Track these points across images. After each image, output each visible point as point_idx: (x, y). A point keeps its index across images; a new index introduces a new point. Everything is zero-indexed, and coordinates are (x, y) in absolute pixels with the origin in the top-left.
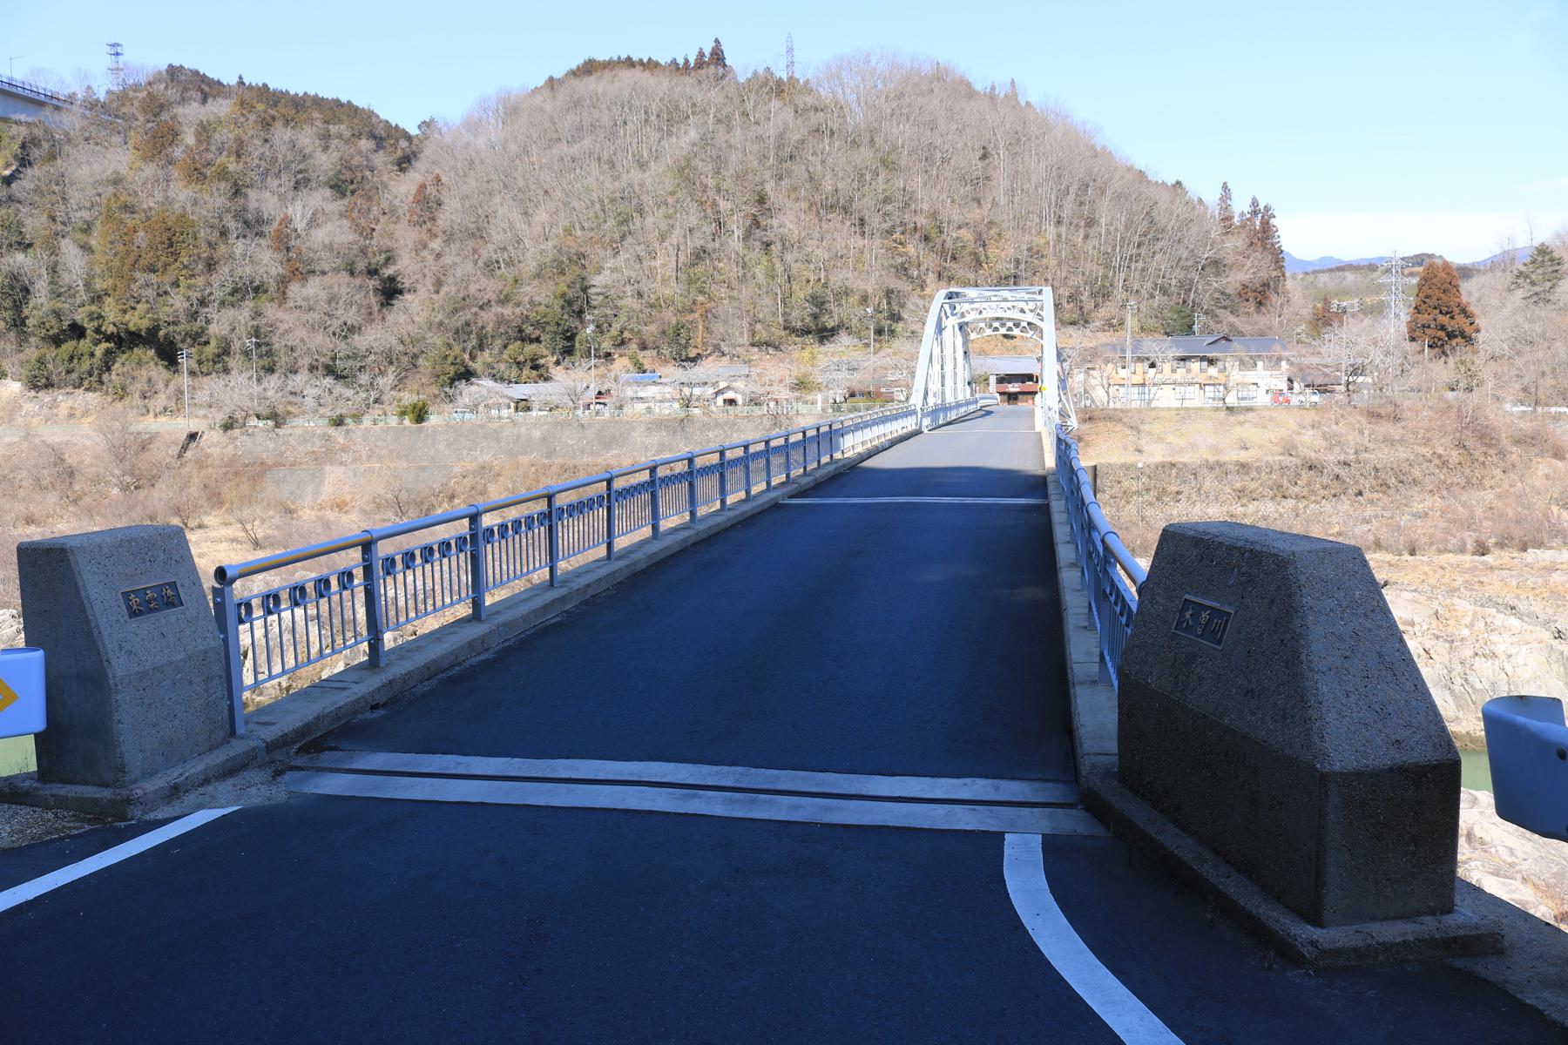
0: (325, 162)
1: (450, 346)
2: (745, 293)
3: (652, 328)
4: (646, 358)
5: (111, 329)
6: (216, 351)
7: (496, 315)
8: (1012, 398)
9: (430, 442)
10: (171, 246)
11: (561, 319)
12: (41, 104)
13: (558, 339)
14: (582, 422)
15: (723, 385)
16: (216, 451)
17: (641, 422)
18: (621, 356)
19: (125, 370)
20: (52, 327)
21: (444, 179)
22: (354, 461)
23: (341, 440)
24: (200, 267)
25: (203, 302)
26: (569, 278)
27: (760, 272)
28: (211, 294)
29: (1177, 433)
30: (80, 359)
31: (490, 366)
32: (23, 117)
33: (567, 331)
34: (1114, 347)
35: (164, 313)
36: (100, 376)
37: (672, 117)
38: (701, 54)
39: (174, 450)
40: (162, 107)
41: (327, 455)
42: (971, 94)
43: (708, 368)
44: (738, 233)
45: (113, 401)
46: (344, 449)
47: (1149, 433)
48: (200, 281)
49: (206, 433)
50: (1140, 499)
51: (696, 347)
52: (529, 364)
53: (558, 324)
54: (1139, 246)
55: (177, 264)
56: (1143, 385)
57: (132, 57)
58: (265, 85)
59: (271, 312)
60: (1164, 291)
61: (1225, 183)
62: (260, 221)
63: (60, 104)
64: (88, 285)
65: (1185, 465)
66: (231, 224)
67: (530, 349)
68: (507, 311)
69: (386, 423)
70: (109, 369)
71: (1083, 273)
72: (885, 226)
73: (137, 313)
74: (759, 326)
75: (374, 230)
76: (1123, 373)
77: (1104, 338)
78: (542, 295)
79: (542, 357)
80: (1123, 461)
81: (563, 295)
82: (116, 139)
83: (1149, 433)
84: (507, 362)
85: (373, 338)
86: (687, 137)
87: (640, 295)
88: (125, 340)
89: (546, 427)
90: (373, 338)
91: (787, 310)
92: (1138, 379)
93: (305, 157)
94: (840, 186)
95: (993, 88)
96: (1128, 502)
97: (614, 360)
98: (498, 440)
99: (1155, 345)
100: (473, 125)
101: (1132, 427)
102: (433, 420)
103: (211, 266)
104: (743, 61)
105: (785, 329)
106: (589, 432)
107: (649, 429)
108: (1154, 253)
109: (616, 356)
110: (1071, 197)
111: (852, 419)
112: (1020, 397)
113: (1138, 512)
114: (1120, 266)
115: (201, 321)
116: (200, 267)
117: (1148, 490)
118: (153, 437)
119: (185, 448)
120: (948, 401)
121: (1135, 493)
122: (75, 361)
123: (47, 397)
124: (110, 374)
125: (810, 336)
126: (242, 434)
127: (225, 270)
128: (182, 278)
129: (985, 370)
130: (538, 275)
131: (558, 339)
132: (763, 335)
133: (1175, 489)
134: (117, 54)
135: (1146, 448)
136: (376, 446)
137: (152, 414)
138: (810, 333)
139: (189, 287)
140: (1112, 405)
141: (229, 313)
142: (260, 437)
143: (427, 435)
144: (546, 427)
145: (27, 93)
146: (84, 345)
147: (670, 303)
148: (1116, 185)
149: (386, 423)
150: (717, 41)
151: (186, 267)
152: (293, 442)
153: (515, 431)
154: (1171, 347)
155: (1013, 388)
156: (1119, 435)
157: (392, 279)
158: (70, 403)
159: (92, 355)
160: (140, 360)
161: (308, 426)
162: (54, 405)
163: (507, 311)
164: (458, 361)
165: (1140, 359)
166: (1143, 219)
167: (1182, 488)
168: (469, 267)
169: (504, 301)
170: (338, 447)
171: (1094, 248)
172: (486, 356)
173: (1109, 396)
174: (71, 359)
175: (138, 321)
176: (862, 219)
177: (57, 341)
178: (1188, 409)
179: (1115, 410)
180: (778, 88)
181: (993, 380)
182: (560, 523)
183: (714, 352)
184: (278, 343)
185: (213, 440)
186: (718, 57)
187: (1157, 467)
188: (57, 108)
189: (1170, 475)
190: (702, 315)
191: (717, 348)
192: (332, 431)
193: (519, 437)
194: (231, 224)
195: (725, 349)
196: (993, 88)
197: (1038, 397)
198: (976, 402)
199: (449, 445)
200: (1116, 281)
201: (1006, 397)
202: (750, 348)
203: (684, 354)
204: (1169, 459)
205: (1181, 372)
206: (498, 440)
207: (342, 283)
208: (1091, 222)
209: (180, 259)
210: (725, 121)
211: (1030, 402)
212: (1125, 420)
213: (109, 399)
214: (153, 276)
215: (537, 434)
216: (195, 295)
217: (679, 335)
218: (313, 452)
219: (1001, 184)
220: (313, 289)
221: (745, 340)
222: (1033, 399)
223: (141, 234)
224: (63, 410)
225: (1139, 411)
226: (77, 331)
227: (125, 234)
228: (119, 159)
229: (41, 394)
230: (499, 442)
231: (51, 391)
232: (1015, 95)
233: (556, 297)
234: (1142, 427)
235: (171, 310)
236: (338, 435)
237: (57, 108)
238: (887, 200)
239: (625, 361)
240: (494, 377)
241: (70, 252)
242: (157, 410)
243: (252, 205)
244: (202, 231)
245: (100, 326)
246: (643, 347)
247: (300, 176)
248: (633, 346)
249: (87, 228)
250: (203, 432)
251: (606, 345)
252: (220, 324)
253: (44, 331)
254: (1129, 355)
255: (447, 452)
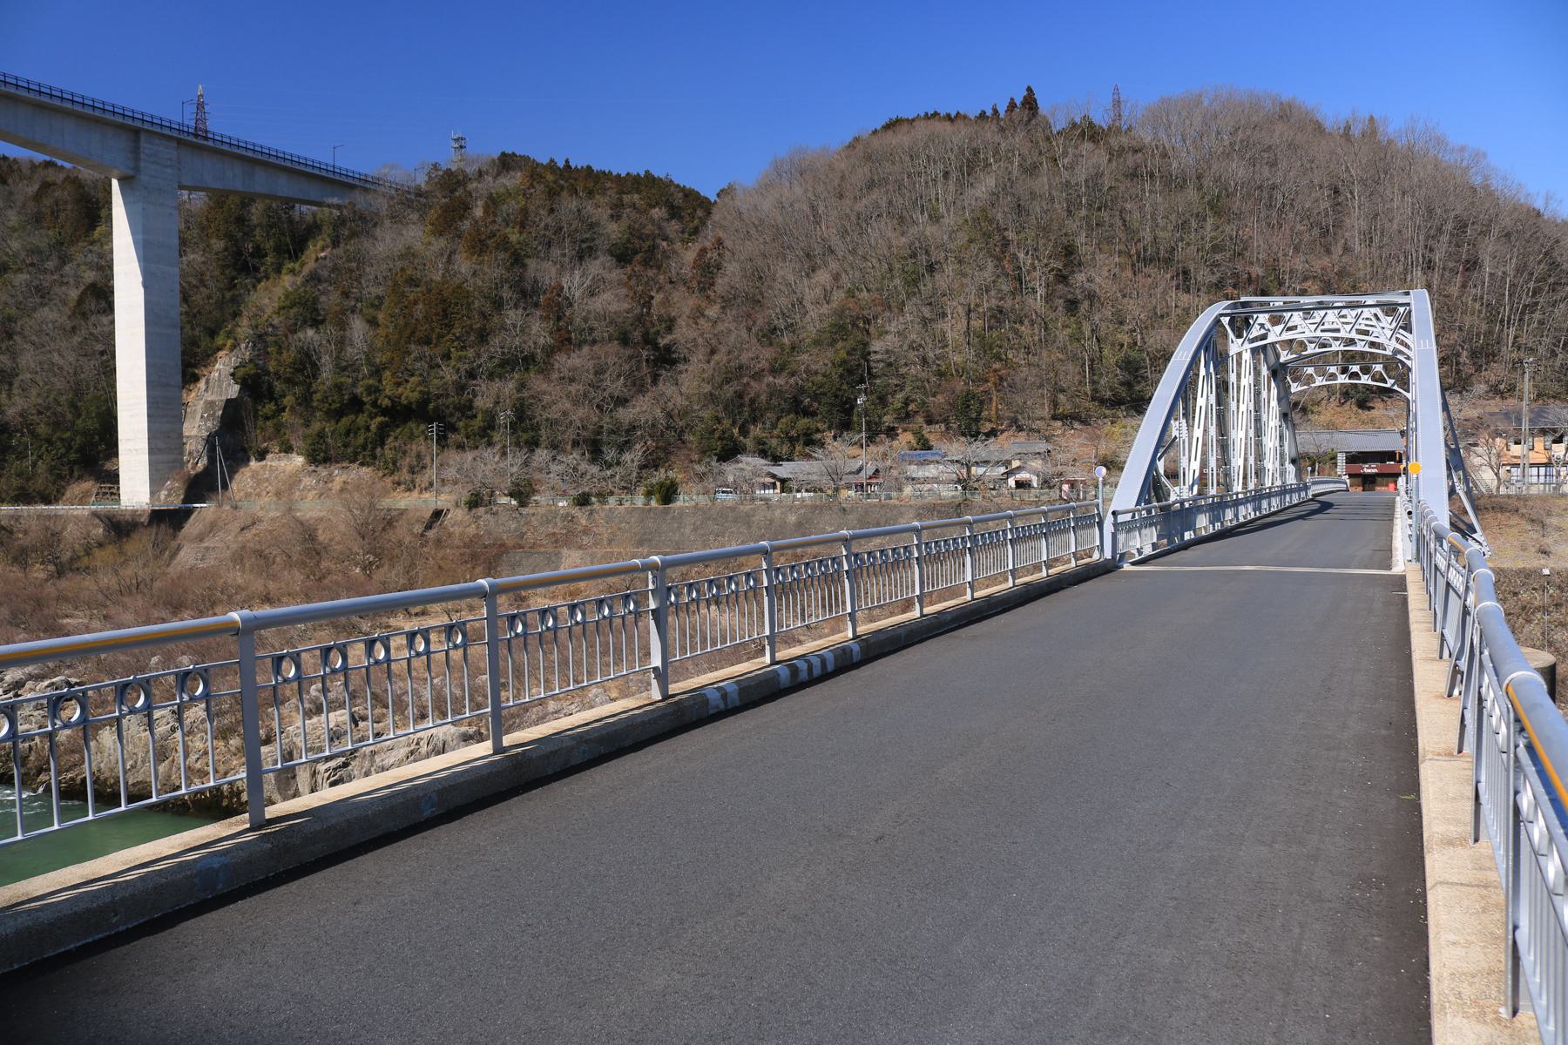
0: (614, 231)
1: (718, 420)
2: (1045, 357)
3: (940, 399)
4: (932, 433)
5: (386, 402)
6: (482, 424)
7: (768, 385)
8: (1368, 482)
9: (676, 525)
10: (445, 316)
11: (839, 389)
12: (352, 187)
14: (844, 505)
15: (1015, 464)
16: (457, 530)
17: (911, 506)
19: (397, 444)
20: (333, 401)
21: (728, 243)
22: (595, 544)
23: (584, 522)
24: (472, 338)
25: (472, 375)
26: (851, 343)
27: (1063, 336)
28: (480, 366)
30: (356, 433)
31: (760, 442)
32: (335, 201)
33: (846, 403)
34: (1507, 415)
35: (435, 385)
36: (374, 449)
37: (972, 164)
39: (418, 529)
40: (459, 183)
41: (568, 537)
42: (1319, 128)
43: (1007, 445)
44: (1041, 292)
45: (384, 475)
46: (586, 531)
47: (1559, 529)
48: (471, 353)
49: (452, 511)
50: (1546, 617)
51: (990, 421)
53: (836, 396)
54: (1534, 294)
55: (450, 336)
56: (1548, 465)
57: (473, 150)
58: (589, 168)
59: (538, 383)
62: (536, 290)
63: (368, 186)
64: (369, 362)
66: (506, 293)
67: (804, 422)
68: (780, 381)
69: (632, 503)
70: (383, 444)
71: (1460, 329)
72: (1214, 279)
73: (409, 386)
74: (1061, 397)
75: (652, 298)
76: (1516, 450)
77: (1495, 405)
78: (819, 362)
79: (818, 431)
80: (1520, 565)
81: (844, 362)
82: (415, 216)
83: (1559, 529)
84: (779, 437)
85: (642, 409)
86: (985, 185)
87: (924, 361)
88: (399, 414)
90: (642, 409)
91: (1096, 378)
93: (592, 226)
94: (1161, 234)
95: (1348, 128)
96: (1529, 621)
98: (749, 525)
101: (1533, 521)
102: (682, 502)
103: (483, 337)
104: (1057, 110)
105: (1093, 399)
107: (919, 514)
109: (900, 431)
110: (1445, 238)
111: (1045, 513)
113: (1543, 634)
114: (1509, 319)
115: (468, 393)
116: (472, 338)
117: (1557, 605)
118: (402, 512)
119: (429, 527)
120: (1268, 484)
121: (1538, 609)
122: (352, 435)
123: (323, 471)
124: (383, 448)
125: (1123, 407)
126: (486, 513)
127: (495, 341)
128: (452, 350)
130: (817, 343)
132: (1065, 406)
134: (461, 147)
136: (619, 529)
137: (418, 489)
138: (1123, 404)
139: (460, 359)
140: (1503, 490)
141: (497, 384)
142: (503, 517)
143: (673, 518)
145: (343, 179)
146: (361, 419)
147: (961, 371)
148: (1507, 222)
149: (632, 503)
150: (1029, 89)
151: (458, 338)
152: (535, 523)
153: (769, 515)
155: (1369, 469)
156: (1515, 531)
157: (668, 348)
158: (344, 477)
159: (368, 429)
160: (412, 434)
161: (553, 502)
162: (330, 479)
164: (726, 435)
165: (1544, 432)
168: (744, 333)
169: (774, 371)
170: (580, 528)
171: (1475, 300)
173: (1499, 479)
174: (348, 433)
175: (409, 393)
176: (1186, 272)
177: (338, 414)
179: (1509, 496)
180: (1090, 133)
181: (1341, 459)
184: (541, 415)
185: (457, 517)
186: (1030, 102)
188: (366, 190)
192: (576, 511)
194: (506, 293)
196: (1348, 128)
197: (1401, 481)
198: (1306, 488)
199: (695, 529)
201: (1360, 479)
202: (1052, 423)
203: (974, 428)
206: (749, 525)
207: (611, 353)
208: (1472, 265)
209: (453, 331)
210: (1031, 170)
211: (1392, 486)
213: (381, 474)
214: (426, 348)
215: (792, 518)
216: (464, 367)
218: (554, 534)
219: (1356, 222)
220: (577, 360)
221: (1046, 412)
222: (1396, 483)
223: (420, 306)
224: (337, 485)
225: (1543, 498)
226: (356, 404)
227: (406, 307)
228: (415, 234)
229: (320, 468)
230: (750, 527)
231: (328, 465)
232: (1374, 132)
234: (1548, 521)
235: (441, 383)
236: (581, 515)
237: (366, 190)
238: (1216, 249)
240: (763, 454)
241: (358, 327)
242: (423, 486)
243: (531, 273)
244: (476, 302)
245: (376, 400)
246: (930, 422)
247: (584, 246)
248: (920, 419)
249: (377, 303)
250: (448, 510)
251: (888, 420)
252: (486, 395)
253: (327, 405)
254: (1525, 426)
255: (692, 538)
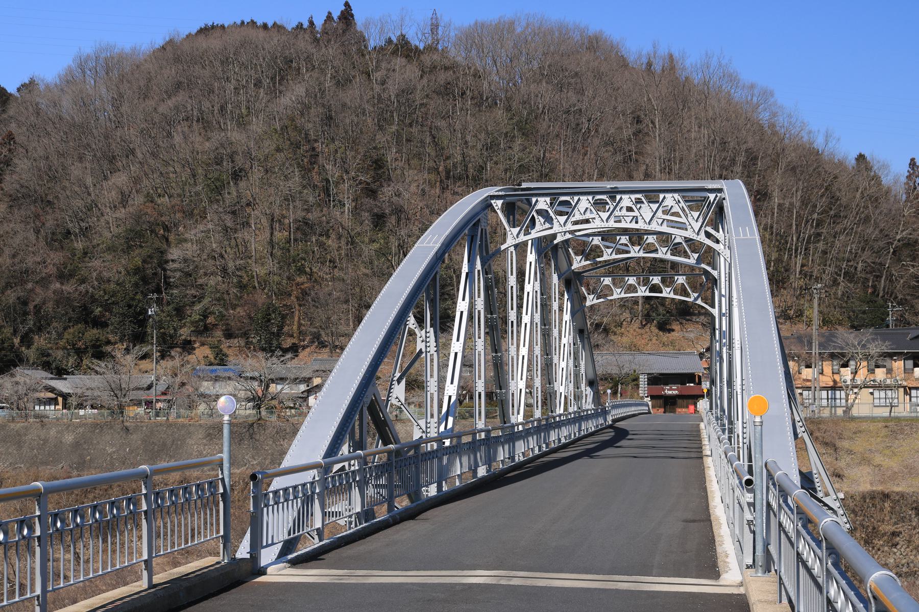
3: (240, 311)
8: (669, 403)
13: (127, 323)
17: (200, 425)
18: (203, 344)
29: (887, 452)
38: (329, 17)
51: (292, 336)
52: (91, 351)
60: (850, 276)
61: (913, 160)
65: (902, 495)
67: (93, 333)
68: (68, 288)
83: (850, 452)
84: (64, 348)
89: (81, 430)
92: (827, 380)
97: (194, 349)
98: (19, 445)
99: (846, 337)
100: (69, 81)
106: (134, 437)
107: (209, 435)
108: (836, 233)
112: (679, 401)
129: (634, 367)
131: (127, 323)
133: (888, 528)
135: (846, 472)
144: (81, 430)
148: (792, 156)
150: (347, 4)
153: (43, 434)
154: (873, 340)
155: (671, 390)
163: (68, 288)
165: (832, 356)
166: (822, 196)
167: (899, 527)
169: (62, 277)
172: (40, 341)
178: (898, 419)
181: (643, 380)
182: (265, 509)
183: (313, 342)
187: (864, 498)
189: (882, 510)
190: (298, 298)
191: (316, 337)
193: (46, 441)
195: (324, 338)
198: (605, 413)
200: (793, 264)
201: (661, 402)
204: (880, 488)
205: (880, 374)
206: (19, 445)
212: (818, 434)
215: (69, 438)
217: (269, 320)
233: (128, 273)
234: (839, 444)
239: (206, 351)
246: (229, 335)
248: (219, 333)
251: (185, 333)
